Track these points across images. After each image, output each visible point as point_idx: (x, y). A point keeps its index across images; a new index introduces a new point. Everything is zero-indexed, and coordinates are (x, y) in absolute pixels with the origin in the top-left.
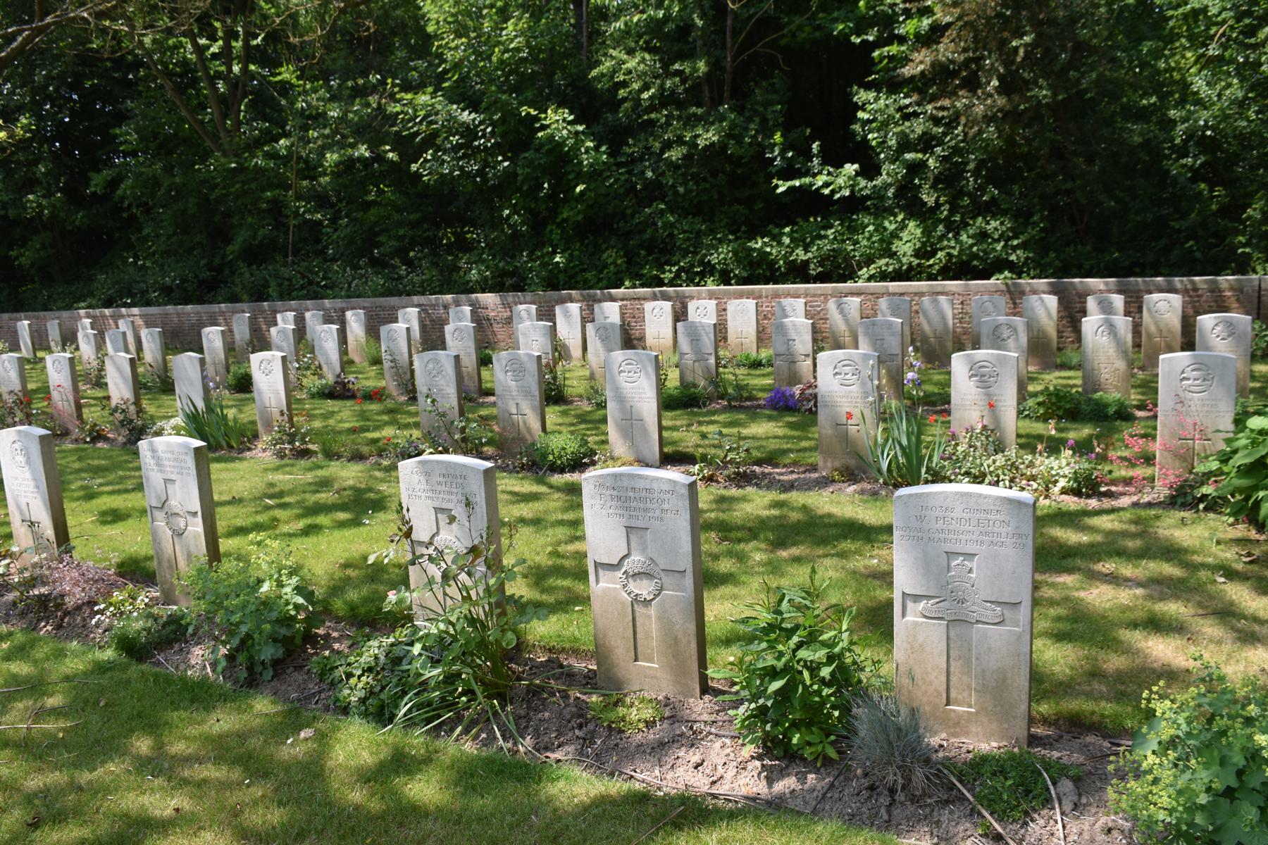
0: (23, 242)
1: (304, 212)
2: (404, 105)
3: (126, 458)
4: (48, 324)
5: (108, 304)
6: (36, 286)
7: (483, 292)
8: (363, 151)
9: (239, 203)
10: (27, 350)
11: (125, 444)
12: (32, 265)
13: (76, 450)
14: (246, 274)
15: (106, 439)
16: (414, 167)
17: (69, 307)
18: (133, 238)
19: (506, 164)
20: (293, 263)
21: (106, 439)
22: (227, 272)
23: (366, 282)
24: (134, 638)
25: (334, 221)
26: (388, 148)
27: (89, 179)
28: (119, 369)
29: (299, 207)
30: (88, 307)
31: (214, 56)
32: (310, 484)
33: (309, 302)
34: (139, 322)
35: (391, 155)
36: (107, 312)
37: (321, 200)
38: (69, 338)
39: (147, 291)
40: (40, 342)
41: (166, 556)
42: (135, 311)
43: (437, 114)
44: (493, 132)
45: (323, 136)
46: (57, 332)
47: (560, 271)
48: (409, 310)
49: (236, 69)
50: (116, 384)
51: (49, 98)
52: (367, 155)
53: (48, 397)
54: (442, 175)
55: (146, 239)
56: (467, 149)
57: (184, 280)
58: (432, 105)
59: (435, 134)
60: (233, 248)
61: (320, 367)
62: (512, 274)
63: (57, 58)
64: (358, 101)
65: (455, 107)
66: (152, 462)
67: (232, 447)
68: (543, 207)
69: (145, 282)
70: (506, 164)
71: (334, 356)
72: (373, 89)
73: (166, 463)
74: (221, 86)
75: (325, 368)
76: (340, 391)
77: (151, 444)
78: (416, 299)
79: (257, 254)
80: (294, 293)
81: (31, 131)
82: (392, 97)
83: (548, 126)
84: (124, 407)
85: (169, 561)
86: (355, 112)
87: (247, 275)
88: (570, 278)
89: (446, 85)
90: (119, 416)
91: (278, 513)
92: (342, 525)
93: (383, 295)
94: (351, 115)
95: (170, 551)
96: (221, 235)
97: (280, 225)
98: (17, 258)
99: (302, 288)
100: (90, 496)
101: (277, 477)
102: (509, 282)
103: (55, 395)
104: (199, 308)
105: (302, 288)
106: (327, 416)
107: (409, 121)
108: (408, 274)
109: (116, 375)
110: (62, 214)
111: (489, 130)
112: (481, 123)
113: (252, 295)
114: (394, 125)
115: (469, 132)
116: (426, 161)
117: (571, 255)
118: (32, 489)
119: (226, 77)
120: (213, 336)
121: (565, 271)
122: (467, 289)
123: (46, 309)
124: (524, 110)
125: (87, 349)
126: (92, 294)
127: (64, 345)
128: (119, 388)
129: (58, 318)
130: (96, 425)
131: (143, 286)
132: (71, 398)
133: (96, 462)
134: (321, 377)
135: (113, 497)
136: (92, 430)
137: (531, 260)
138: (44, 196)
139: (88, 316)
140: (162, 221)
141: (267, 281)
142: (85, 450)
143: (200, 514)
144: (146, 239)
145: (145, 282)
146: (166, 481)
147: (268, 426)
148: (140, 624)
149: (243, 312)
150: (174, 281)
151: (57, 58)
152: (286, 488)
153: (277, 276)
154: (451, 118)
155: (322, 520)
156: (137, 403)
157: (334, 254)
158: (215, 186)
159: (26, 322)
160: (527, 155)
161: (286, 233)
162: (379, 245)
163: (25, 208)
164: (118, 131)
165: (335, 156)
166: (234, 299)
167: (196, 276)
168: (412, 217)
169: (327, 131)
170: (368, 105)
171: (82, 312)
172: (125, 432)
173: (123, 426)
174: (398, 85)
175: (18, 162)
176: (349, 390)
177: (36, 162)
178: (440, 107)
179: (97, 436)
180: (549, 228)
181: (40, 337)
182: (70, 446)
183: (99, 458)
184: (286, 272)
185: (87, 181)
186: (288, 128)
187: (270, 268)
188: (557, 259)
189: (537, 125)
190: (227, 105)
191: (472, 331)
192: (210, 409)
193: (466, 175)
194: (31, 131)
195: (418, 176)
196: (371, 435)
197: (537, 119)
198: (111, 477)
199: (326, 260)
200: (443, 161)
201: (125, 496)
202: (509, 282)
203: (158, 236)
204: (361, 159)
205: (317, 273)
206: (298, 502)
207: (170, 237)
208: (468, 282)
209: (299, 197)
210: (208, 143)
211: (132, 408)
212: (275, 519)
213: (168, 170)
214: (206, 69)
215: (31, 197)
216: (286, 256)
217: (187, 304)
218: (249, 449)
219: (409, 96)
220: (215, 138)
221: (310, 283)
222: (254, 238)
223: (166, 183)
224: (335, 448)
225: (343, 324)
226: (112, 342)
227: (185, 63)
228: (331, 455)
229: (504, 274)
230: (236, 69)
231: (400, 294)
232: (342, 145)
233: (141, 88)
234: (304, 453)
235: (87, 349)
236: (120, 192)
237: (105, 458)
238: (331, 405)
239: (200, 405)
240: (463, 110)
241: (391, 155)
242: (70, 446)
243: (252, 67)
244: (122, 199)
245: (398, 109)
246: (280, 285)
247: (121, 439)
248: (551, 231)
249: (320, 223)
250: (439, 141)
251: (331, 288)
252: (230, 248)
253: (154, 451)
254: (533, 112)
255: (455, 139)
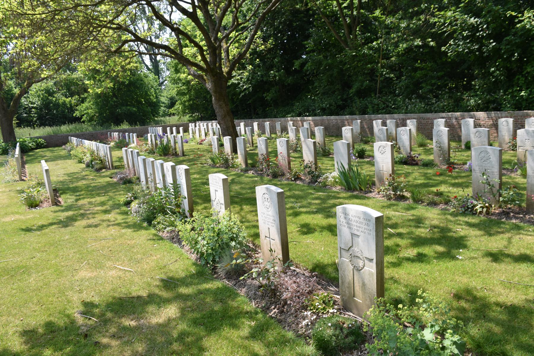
0: (268, 91)
1: (385, 74)
2: (439, 18)
3: (310, 191)
4: (276, 124)
5: (299, 115)
6: (272, 108)
7: (477, 111)
8: (418, 42)
9: (356, 70)
10: (268, 134)
11: (309, 183)
12: (271, 99)
13: (288, 184)
14: (358, 103)
15: (301, 180)
16: (443, 49)
17: (284, 116)
18: (310, 87)
19: (494, 44)
20: (379, 97)
21: (301, 180)
22: (349, 101)
23: (415, 106)
24: (328, 341)
25: (398, 78)
26: (430, 40)
27: (294, 63)
28: (308, 147)
29: (383, 71)
30: (292, 116)
31: (345, 7)
32: (410, 220)
33: (387, 115)
34: (312, 123)
35: (432, 43)
36: (299, 118)
37: (392, 68)
38: (284, 129)
39: (315, 110)
40: (273, 130)
41: (347, 281)
42: (310, 118)
43: (457, 20)
44: (487, 27)
45: (398, 37)
46: (280, 127)
47: (523, 100)
48: (440, 120)
49: (355, 13)
50: (306, 153)
51: (280, 32)
52: (420, 44)
53: (276, 156)
54: (458, 52)
55: (316, 87)
56: (473, 38)
57: (331, 105)
58: (454, 17)
59: (455, 31)
60: (353, 91)
61: (399, 148)
62: (493, 102)
63: (284, 14)
64: (415, 18)
65: (466, 16)
66: (344, 221)
67: (362, 190)
68: (515, 66)
69: (314, 106)
70: (494, 44)
71: (407, 143)
72: (422, 12)
73: (353, 223)
74: (348, 20)
75: (402, 149)
76: (410, 161)
77: (345, 209)
78: (444, 115)
79: (362, 94)
80: (380, 111)
81: (273, 45)
82: (433, 15)
83: (523, 21)
84: (310, 165)
85: (349, 284)
86: (413, 24)
87: (358, 103)
88: (529, 104)
89: (462, 5)
90: (308, 170)
91: (398, 241)
92: (440, 256)
93: (423, 112)
94: (411, 25)
95: (351, 278)
96: (347, 85)
97: (372, 80)
98: (266, 97)
99: (383, 109)
100: (296, 214)
101: (390, 213)
102: (491, 106)
103: (280, 157)
104: (337, 117)
105: (383, 109)
106: (407, 175)
107: (442, 25)
108: (436, 102)
109: (307, 149)
110: (283, 78)
111: (485, 26)
112: (481, 23)
113: (360, 112)
114: (434, 28)
115: (474, 29)
116: (450, 45)
117: (530, 91)
118: (271, 221)
119: (351, 16)
120: (346, 131)
121: (526, 100)
122: (468, 110)
123: (276, 117)
124: (509, 13)
125: (292, 135)
126: (293, 111)
127: (282, 132)
128: (308, 156)
129: (280, 121)
130: (296, 172)
131: (313, 107)
132: (286, 160)
133: (297, 193)
134: (400, 153)
135: (307, 216)
136: (295, 175)
137: (505, 94)
138: (277, 72)
139: (291, 121)
140: (322, 80)
141: (367, 105)
142: (291, 184)
143: (375, 261)
144: (316, 87)
145: (314, 106)
146: (353, 235)
147: (381, 181)
148: (330, 332)
149: (356, 119)
150: (326, 105)
151: (284, 14)
152: (399, 221)
153: (371, 103)
154: (465, 21)
155: (427, 250)
156: (316, 164)
157: (399, 93)
158: (345, 64)
159: (268, 123)
160: (508, 38)
161: (376, 83)
162: (421, 88)
163: (270, 77)
164: (306, 42)
165: (405, 46)
166: (352, 113)
167: (336, 104)
168: (439, 74)
169: (400, 34)
170: (420, 20)
171: (289, 118)
172: (309, 177)
173: (309, 174)
174: (437, 8)
175: (268, 58)
176: (414, 161)
177: (274, 58)
178: (457, 17)
179: (297, 178)
180: (517, 77)
181: (273, 128)
182: (286, 182)
183: (298, 190)
184: (376, 101)
185: (293, 65)
186: (379, 35)
187: (369, 99)
188: (523, 93)
189: (517, 21)
190: (351, 28)
191: (447, 132)
192: (350, 168)
193: (471, 52)
194: (273, 45)
195: (445, 53)
196: (434, 189)
197: (516, 17)
198: (305, 203)
199: (396, 96)
200: (459, 45)
201: (312, 216)
202: (491, 106)
203: (321, 86)
204: (418, 47)
205: (390, 102)
206: (408, 233)
207: (325, 86)
208: (468, 106)
209: (382, 67)
210: (343, 45)
211: (314, 166)
212: (398, 245)
213: (326, 57)
214: (342, 12)
215: (272, 72)
216: (376, 94)
217: (331, 116)
218: (371, 192)
219: (442, 13)
220: (346, 42)
221: (388, 106)
222: (362, 86)
223: (324, 63)
224: (419, 196)
225: (253, 126)
226: (302, 132)
227: (332, 11)
228: (417, 201)
229: (489, 102)
230: (355, 13)
231: (431, 112)
232: (406, 40)
233: (315, 24)
234: (402, 198)
235: (292, 135)
236: (305, 68)
237: (302, 191)
238: (406, 168)
239: (346, 167)
240: (471, 18)
241: (432, 43)
242: (286, 182)
243: (362, 11)
244: (307, 70)
245: (436, 20)
246: (373, 107)
247: (307, 180)
248: (519, 79)
249: (391, 79)
250: (455, 36)
251: (397, 109)
252: (351, 91)
253: (345, 213)
254: (514, 14)
255: (465, 34)
